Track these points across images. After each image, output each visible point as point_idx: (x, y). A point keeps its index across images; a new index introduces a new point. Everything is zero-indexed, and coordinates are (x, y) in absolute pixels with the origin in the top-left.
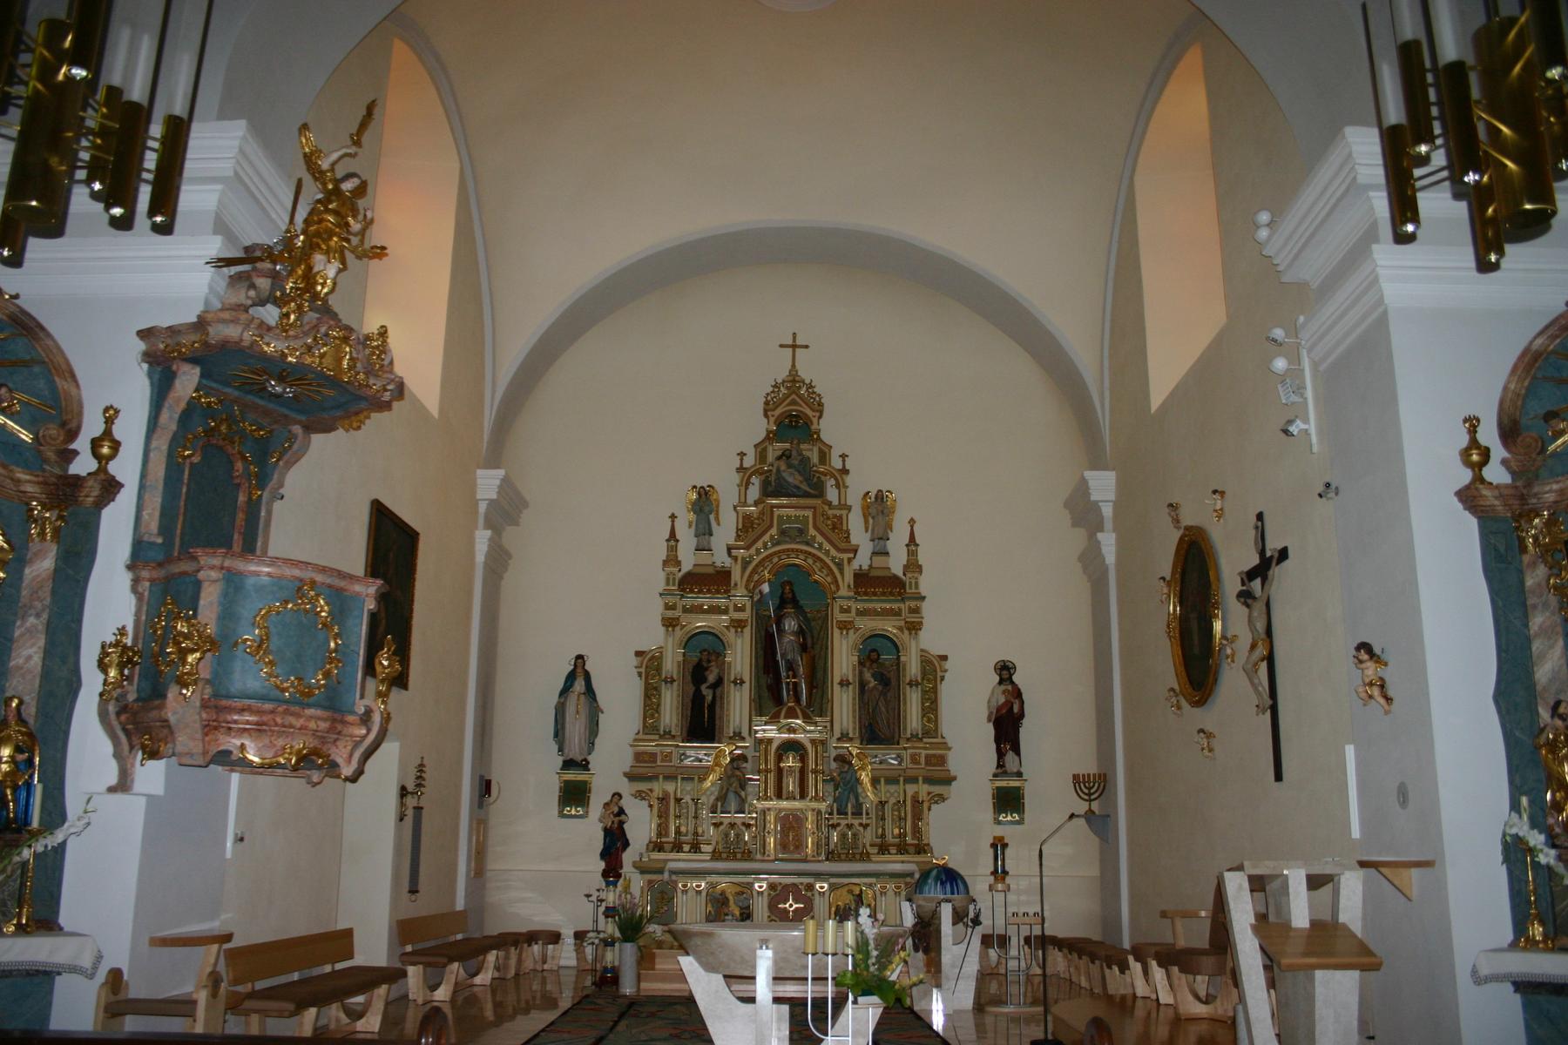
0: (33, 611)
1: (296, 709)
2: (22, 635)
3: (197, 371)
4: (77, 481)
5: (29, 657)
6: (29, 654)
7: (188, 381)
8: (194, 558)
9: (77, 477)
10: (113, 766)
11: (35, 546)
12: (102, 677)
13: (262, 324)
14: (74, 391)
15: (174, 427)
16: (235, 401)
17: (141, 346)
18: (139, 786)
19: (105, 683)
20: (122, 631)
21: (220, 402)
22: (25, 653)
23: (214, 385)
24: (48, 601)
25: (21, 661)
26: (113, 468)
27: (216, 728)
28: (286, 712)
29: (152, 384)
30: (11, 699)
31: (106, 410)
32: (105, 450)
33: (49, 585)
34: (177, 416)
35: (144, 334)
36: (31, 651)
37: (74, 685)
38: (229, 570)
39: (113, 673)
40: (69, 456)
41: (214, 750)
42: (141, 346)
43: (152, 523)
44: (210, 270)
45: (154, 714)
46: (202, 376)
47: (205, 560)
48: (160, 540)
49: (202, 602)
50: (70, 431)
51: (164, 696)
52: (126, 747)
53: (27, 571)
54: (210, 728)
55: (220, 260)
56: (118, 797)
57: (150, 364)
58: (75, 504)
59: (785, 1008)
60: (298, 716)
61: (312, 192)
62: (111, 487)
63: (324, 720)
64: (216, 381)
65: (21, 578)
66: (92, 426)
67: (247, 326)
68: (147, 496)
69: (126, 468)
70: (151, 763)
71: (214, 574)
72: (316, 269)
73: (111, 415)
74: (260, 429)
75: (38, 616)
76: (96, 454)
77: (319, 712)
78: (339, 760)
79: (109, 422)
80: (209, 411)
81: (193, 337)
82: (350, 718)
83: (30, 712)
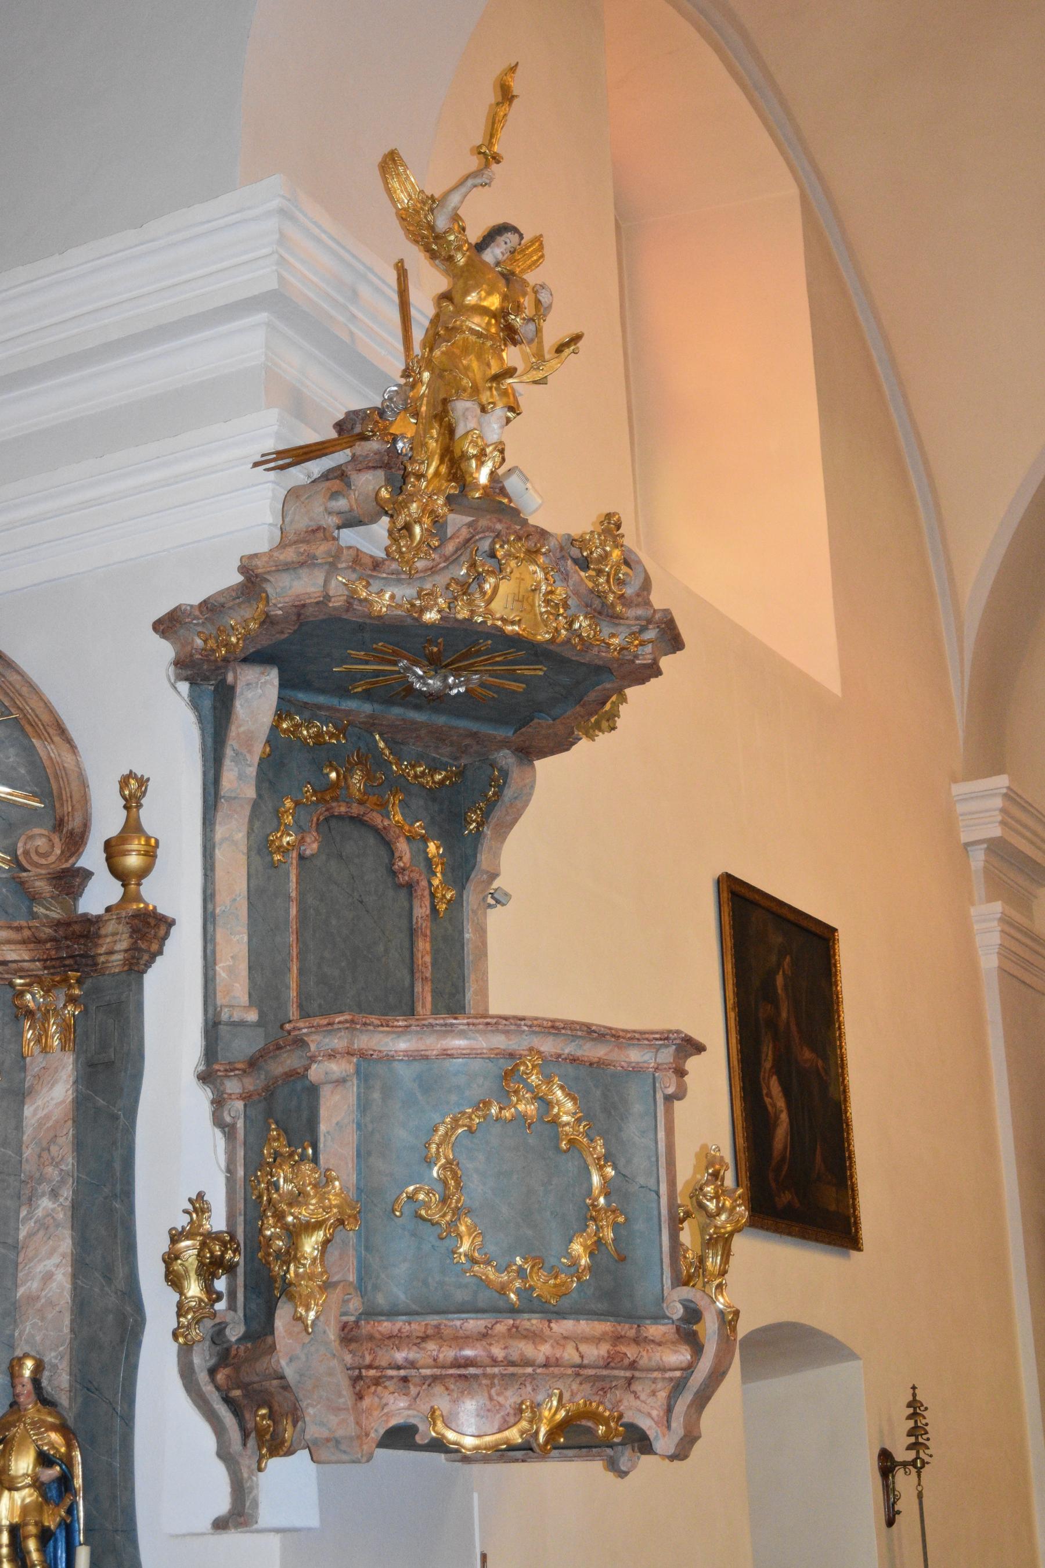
0: (45, 1187)
1: (533, 1322)
2: (31, 1235)
3: (272, 677)
4: (87, 929)
6: (48, 1271)
7: (258, 696)
8: (300, 1043)
10: (219, 1475)
11: (36, 1063)
13: (357, 558)
14: (68, 760)
15: (251, 793)
16: (371, 725)
18: (267, 1514)
19: (181, 1310)
20: (199, 1205)
21: (342, 730)
23: (321, 699)
24: (69, 1162)
25: (35, 1285)
26: (155, 894)
27: (377, 1382)
28: (516, 1333)
29: (200, 719)
30: (20, 1361)
31: (124, 782)
34: (252, 771)
35: (167, 625)
36: (49, 1264)
38: (363, 1055)
39: (194, 1289)
40: (71, 881)
41: (379, 1428)
47: (316, 1043)
49: (323, 1128)
50: (71, 833)
53: (28, 1111)
54: (362, 1382)
55: (280, 454)
56: (233, 1538)
58: (92, 967)
60: (535, 1337)
61: (429, 283)
62: (149, 930)
63: (597, 1340)
64: (322, 691)
65: (19, 1127)
66: (107, 819)
67: (332, 567)
69: (175, 889)
70: (274, 1464)
71: (337, 1068)
72: (460, 431)
73: (133, 791)
74: (433, 770)
75: (54, 1194)
76: (117, 872)
77: (584, 1326)
78: (645, 1424)
79: (132, 802)
80: (320, 753)
81: (247, 612)
82: (654, 1330)
83: (60, 1382)
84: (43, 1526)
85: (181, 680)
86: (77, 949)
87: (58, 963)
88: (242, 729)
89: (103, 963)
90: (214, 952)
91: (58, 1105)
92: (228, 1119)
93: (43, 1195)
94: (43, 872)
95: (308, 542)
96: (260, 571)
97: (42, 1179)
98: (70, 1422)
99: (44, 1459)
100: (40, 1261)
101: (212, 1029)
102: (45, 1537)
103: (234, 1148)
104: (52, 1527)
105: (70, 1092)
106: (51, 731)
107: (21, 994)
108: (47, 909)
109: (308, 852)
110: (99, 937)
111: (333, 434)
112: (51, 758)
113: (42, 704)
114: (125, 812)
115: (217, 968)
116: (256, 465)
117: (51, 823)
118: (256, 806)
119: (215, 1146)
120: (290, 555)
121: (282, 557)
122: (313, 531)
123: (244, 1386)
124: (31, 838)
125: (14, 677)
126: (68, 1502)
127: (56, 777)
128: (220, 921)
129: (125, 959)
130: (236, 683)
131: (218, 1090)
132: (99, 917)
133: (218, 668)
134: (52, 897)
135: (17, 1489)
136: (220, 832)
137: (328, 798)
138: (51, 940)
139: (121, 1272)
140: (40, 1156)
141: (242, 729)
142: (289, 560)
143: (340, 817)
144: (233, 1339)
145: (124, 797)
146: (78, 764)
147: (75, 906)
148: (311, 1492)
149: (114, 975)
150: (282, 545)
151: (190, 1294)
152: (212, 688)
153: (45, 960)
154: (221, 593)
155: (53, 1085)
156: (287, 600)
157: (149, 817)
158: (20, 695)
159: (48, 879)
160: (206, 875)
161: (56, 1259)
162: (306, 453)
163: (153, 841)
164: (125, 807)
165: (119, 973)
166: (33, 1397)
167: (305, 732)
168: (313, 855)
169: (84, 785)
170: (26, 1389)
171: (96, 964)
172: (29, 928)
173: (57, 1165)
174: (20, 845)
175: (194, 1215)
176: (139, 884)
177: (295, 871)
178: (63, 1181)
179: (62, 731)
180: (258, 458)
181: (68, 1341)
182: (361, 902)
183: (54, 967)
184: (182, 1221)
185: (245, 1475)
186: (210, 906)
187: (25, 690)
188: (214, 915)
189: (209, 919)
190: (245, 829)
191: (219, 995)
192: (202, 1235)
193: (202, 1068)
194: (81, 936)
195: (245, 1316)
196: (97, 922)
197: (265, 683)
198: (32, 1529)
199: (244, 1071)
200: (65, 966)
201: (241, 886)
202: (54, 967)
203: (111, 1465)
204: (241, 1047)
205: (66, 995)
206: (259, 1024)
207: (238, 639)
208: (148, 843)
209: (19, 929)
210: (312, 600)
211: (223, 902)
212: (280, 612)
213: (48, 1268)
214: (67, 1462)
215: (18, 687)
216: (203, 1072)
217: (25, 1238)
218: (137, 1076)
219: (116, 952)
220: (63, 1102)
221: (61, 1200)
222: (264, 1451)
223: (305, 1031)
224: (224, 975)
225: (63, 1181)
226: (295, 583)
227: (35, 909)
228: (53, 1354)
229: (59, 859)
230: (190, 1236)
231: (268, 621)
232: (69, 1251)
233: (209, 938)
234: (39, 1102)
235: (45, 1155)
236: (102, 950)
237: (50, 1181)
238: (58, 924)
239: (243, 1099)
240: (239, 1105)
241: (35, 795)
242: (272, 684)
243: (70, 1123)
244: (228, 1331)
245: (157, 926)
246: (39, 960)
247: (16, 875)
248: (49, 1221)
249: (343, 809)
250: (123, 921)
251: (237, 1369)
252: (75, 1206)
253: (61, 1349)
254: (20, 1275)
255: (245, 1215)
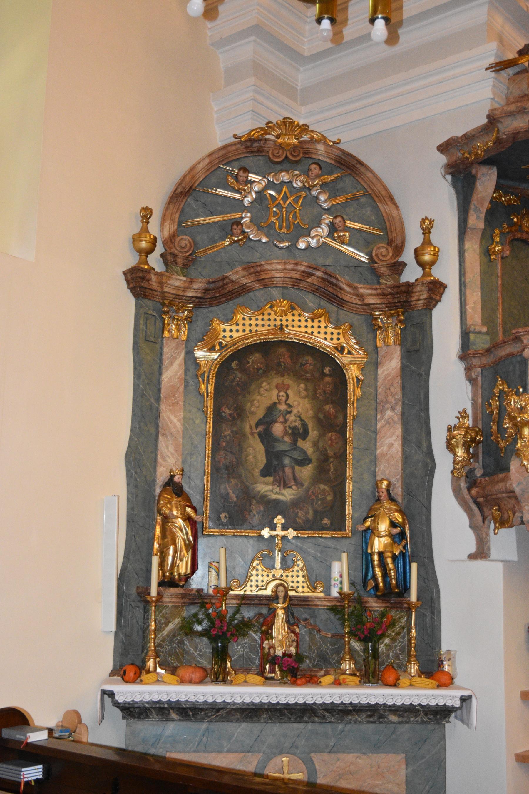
0: (388, 406)
2: (382, 427)
5: (391, 445)
9: (408, 285)
12: (451, 456)
14: (394, 212)
17: (443, 159)
18: (494, 553)
20: (463, 415)
22: (387, 441)
23: (511, 183)
24: (399, 395)
25: (385, 449)
26: (438, 273)
29: (457, 192)
30: (381, 481)
31: (423, 221)
32: (427, 258)
33: (398, 380)
34: (483, 216)
35: (443, 148)
36: (391, 440)
37: (430, 468)
39: (460, 452)
40: (398, 267)
42: (443, 159)
43: (475, 317)
44: (491, 75)
45: (500, 486)
46: (499, 177)
48: (484, 329)
50: (396, 247)
51: (508, 469)
52: (479, 518)
53: (380, 371)
55: (497, 64)
56: (479, 564)
57: (452, 174)
59: (187, 521)
62: (437, 288)
66: (414, 239)
68: (468, 292)
69: (447, 271)
75: (393, 409)
76: (421, 264)
80: (510, 209)
83: (398, 491)
84: (393, 553)
85: (448, 174)
86: (403, 298)
87: (393, 305)
88: (479, 196)
89: (414, 305)
90: (465, 301)
91: (393, 369)
92: (474, 376)
93: (388, 409)
94: (385, 264)
95: (520, 102)
96: (497, 116)
97: (387, 402)
98: (403, 509)
99: (393, 525)
100: (386, 439)
101: (465, 335)
102: (394, 558)
103: (476, 389)
104: (397, 554)
105: (399, 363)
106: (386, 199)
107: (376, 319)
108: (386, 281)
109: (505, 255)
110: (412, 293)
111: (517, 56)
112: (386, 212)
113: (382, 187)
114: (423, 236)
115: (467, 308)
116: (487, 69)
117: (387, 241)
118: (484, 232)
119: (467, 389)
120: (513, 108)
121: (509, 109)
122: (523, 97)
123: (485, 497)
124: (379, 248)
125: (369, 175)
126: (403, 543)
127: (389, 220)
128: (468, 286)
129: (425, 303)
130: (477, 174)
131: (468, 363)
132: (413, 283)
133: (467, 167)
134: (388, 275)
135: (382, 537)
136: (467, 245)
137: (513, 230)
138: (390, 294)
139: (425, 444)
140: (385, 392)
141: (479, 196)
142: (512, 110)
143: (517, 240)
144: (478, 476)
145: (423, 229)
146: (399, 214)
147: (399, 280)
148: (514, 545)
149: (418, 310)
150: (508, 104)
151: (459, 454)
152: (462, 178)
153: (386, 304)
154: (474, 130)
155: (391, 360)
156: (510, 130)
157: (434, 237)
158: (372, 183)
159: (387, 267)
160: (460, 265)
161: (394, 438)
162: (508, 64)
163: (437, 249)
164: (423, 233)
165: (421, 309)
166: (387, 497)
167: (503, 199)
168: (507, 257)
169: (402, 224)
170: (384, 495)
171: (410, 306)
172: (380, 289)
173: (394, 396)
174: (374, 251)
175: (461, 419)
176: (430, 269)
177: (500, 264)
178: (397, 403)
179: (392, 199)
180: (488, 66)
181: (401, 474)
182: (527, 280)
183: (390, 307)
184: (454, 422)
185: (484, 536)
186: (463, 279)
187: (374, 181)
188: (464, 282)
189: (462, 285)
190: (478, 243)
191: (468, 320)
192: (465, 428)
193: (460, 353)
194: (404, 292)
195: (483, 465)
196: (412, 286)
197: (491, 173)
198: (389, 554)
199: (482, 354)
200: (396, 306)
201: (477, 270)
202: (390, 307)
203: (421, 528)
204: (481, 343)
205: (397, 319)
206: (487, 333)
207: (482, 152)
208: (435, 250)
209: (376, 289)
210: (523, 130)
211: (469, 277)
212: (505, 137)
213: (391, 441)
214: (402, 526)
215: (371, 179)
216: (461, 355)
217: (380, 428)
218: (430, 357)
219: (421, 300)
220: (396, 368)
221: (396, 411)
222: (497, 525)
223: (522, 333)
224: (470, 311)
225: (397, 403)
226: (514, 122)
227: (381, 281)
228: (394, 479)
229: (391, 258)
230: (459, 428)
231: (498, 141)
232: (400, 434)
233: (463, 293)
234: (385, 368)
235: (388, 391)
236: (414, 299)
237: (390, 403)
238: (393, 287)
239: (481, 367)
240: (479, 370)
241: (379, 229)
242: (494, 174)
243: (399, 377)
244: (476, 472)
245: (440, 287)
246: (384, 304)
247: (372, 265)
248: (390, 420)
249: (519, 236)
250: (425, 285)
251: (483, 488)
252: (403, 414)
253: (398, 477)
254: (378, 444)
255: (482, 420)
